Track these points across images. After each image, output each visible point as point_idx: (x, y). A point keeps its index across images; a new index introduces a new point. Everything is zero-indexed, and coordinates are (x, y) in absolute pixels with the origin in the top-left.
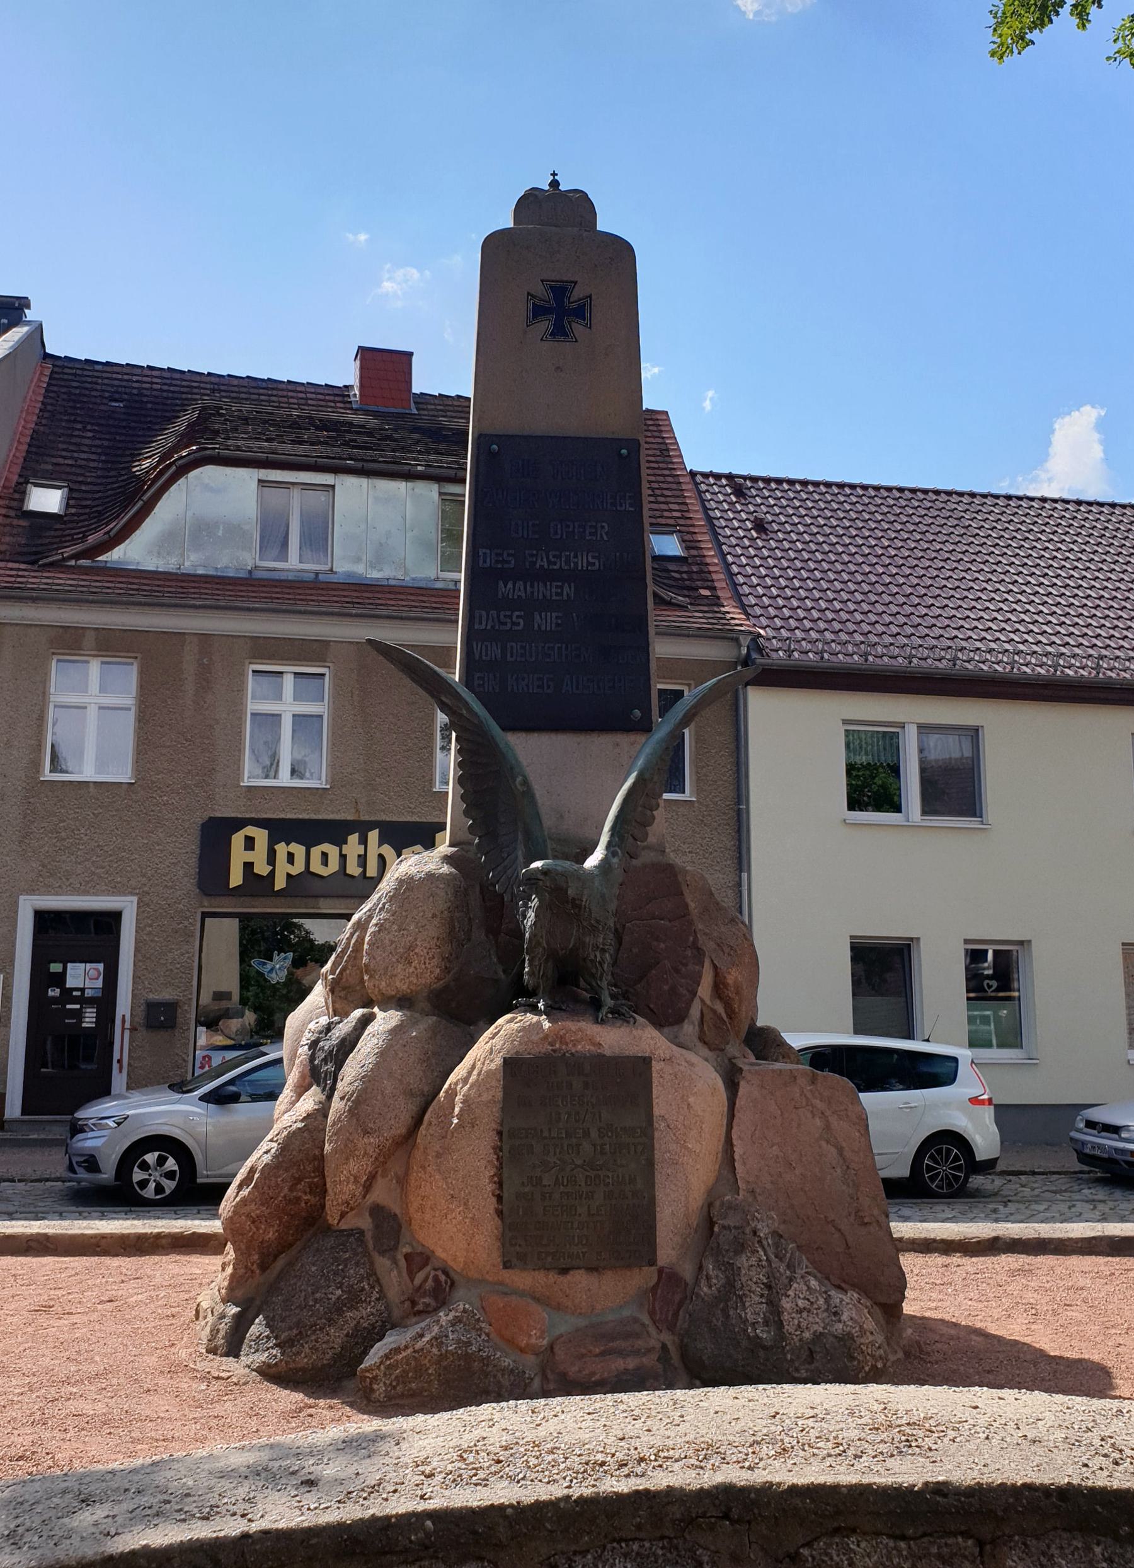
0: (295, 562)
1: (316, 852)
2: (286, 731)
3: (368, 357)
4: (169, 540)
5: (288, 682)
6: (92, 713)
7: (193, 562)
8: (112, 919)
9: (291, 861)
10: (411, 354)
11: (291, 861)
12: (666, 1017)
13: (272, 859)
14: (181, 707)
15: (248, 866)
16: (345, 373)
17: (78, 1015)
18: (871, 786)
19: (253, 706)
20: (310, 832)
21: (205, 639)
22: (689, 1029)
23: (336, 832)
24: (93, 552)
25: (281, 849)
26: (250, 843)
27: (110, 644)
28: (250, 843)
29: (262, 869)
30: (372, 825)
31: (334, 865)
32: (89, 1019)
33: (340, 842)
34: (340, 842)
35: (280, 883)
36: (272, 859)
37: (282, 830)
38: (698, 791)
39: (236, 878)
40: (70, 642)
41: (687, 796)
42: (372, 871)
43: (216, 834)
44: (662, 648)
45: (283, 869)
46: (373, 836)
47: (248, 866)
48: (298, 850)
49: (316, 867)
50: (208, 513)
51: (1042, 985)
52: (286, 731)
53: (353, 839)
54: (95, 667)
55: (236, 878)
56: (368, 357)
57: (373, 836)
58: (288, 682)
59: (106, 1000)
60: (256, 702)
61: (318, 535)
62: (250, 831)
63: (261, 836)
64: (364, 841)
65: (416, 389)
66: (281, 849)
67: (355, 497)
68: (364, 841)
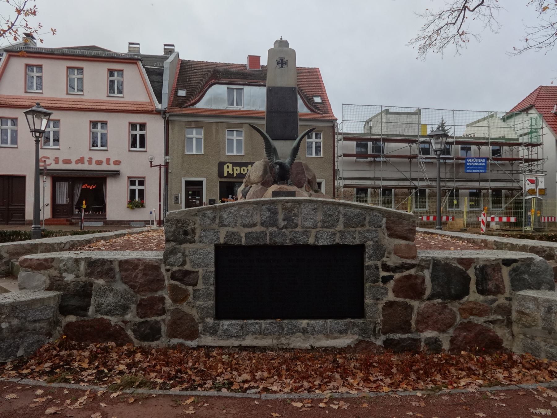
0: (235, 107)
1: (242, 169)
4: (209, 102)
5: (235, 133)
9: (237, 171)
10: (259, 57)
14: (212, 144)
15: (228, 172)
20: (241, 165)
25: (235, 168)
26: (228, 167)
28: (228, 167)
29: (231, 172)
34: (247, 167)
35: (235, 175)
37: (235, 164)
39: (226, 174)
43: (221, 165)
45: (235, 172)
47: (228, 172)
48: (238, 168)
50: (216, 96)
55: (226, 174)
58: (235, 133)
62: (228, 164)
63: (230, 165)
66: (235, 168)
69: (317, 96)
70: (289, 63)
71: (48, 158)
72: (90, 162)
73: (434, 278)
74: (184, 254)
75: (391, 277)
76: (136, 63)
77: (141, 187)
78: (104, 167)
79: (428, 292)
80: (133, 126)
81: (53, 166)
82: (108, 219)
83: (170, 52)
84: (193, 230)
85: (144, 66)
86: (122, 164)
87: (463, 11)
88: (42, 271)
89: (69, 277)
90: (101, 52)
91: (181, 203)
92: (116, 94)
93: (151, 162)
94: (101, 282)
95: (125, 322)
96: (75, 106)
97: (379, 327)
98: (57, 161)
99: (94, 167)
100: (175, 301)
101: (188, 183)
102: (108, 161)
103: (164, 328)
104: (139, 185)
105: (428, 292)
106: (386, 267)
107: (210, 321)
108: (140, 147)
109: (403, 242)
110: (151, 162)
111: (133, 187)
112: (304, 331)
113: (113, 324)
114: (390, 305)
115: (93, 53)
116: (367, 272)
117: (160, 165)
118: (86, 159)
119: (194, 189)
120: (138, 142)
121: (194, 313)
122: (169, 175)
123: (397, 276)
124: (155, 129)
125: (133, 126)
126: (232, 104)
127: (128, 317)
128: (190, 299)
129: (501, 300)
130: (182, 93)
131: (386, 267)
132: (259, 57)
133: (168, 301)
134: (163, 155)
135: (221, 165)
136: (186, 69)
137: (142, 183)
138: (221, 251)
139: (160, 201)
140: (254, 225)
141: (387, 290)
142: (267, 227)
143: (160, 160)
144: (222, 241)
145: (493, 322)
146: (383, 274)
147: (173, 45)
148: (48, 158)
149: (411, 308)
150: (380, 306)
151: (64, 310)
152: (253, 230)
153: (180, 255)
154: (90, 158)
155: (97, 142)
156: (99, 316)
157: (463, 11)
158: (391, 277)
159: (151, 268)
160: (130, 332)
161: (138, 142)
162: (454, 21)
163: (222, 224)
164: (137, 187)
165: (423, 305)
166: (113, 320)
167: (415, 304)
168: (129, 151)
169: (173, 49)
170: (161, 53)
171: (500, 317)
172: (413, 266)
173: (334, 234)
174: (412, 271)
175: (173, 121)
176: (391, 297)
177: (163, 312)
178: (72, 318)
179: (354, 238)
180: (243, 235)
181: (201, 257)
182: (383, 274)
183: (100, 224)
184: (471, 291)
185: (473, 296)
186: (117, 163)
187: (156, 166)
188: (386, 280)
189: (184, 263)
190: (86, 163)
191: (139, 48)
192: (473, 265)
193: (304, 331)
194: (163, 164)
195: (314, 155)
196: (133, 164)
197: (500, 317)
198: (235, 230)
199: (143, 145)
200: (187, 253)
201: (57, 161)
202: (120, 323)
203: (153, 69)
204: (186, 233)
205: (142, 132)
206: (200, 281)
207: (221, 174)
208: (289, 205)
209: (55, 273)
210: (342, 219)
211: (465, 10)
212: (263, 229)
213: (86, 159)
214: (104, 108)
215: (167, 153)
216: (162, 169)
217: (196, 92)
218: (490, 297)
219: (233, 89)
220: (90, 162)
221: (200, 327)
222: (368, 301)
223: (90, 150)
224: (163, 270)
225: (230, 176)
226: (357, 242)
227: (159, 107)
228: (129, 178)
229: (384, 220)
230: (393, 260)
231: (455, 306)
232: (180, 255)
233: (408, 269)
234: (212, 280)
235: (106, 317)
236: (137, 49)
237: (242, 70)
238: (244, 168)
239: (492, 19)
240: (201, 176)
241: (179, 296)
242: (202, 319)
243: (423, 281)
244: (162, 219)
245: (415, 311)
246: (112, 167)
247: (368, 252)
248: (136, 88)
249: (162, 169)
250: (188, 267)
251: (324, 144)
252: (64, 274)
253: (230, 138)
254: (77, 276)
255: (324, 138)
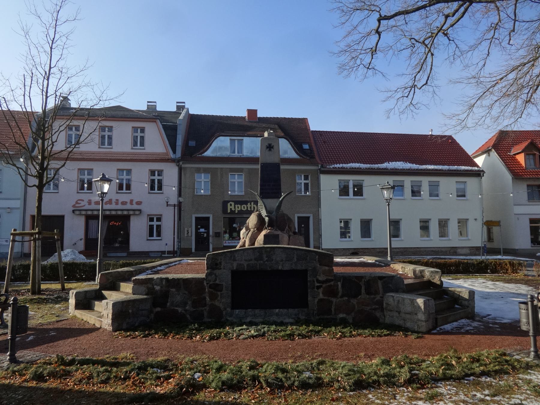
0: (236, 154)
1: (242, 206)
2: (236, 185)
3: (249, 111)
4: (215, 150)
5: (236, 176)
6: (203, 182)
7: (218, 154)
8: (208, 218)
9: (238, 208)
10: (257, 110)
11: (238, 208)
12: (282, 230)
13: (235, 208)
14: (218, 184)
15: (231, 209)
16: (245, 114)
17: (203, 235)
18: (344, 191)
19: (230, 180)
20: (241, 203)
21: (222, 169)
22: (285, 232)
23: (246, 203)
24: (201, 154)
25: (236, 206)
26: (231, 205)
27: (206, 171)
28: (231, 205)
29: (233, 209)
30: (252, 201)
31: (246, 208)
32: (205, 235)
33: (247, 204)
34: (247, 204)
35: (236, 212)
36: (235, 208)
37: (236, 203)
38: (312, 192)
39: (229, 211)
40: (198, 170)
41: (211, 216)
42: (252, 209)
43: (225, 204)
44: (30, 312)
45: (237, 209)
46: (252, 203)
47: (231, 209)
48: (239, 206)
49: (243, 209)
50: (221, 145)
51: (374, 228)
52: (236, 185)
53: (249, 204)
54: (203, 175)
55: (229, 211)
56: (249, 111)
57: (252, 203)
58: (236, 176)
59: (208, 233)
60: (231, 180)
61: (240, 149)
62: (231, 203)
63: (233, 204)
64: (251, 204)
65: (258, 116)
66: (236, 206)
67: (247, 141)
68: (251, 204)
69: (305, 143)
70: (275, 147)
71: (83, 200)
72: (117, 203)
73: (343, 286)
74: (215, 275)
75: (321, 286)
76: (155, 122)
77: (159, 223)
78: (128, 206)
79: (340, 294)
80: (153, 173)
81: (87, 207)
82: (131, 250)
83: (183, 107)
84: (220, 263)
85: (161, 122)
86: (143, 204)
87: (413, 89)
88: (144, 285)
89: (157, 288)
90: (126, 113)
91: (191, 236)
92: (139, 147)
93: (167, 202)
94: (174, 290)
95: (186, 311)
96: (106, 157)
97: (315, 312)
98: (90, 202)
99: (120, 207)
100: (211, 299)
101: (197, 219)
102: (131, 201)
103: (206, 314)
104: (157, 221)
105: (340, 294)
106: (318, 281)
107: (229, 310)
108: (158, 190)
109: (327, 268)
110: (167, 202)
111: (152, 223)
112: (277, 315)
113: (180, 311)
114: (321, 300)
115: (120, 113)
116: (309, 284)
117: (175, 205)
118: (114, 201)
119: (202, 222)
120: (156, 185)
121: (221, 306)
122: (182, 212)
123: (324, 285)
124: (170, 174)
125: (153, 173)
126: (234, 152)
127: (187, 308)
128: (219, 298)
129: (378, 297)
130: (192, 143)
131: (318, 281)
132: (257, 110)
133: (208, 299)
134: (177, 196)
135: (225, 204)
136: (195, 121)
137: (159, 220)
138: (235, 274)
139: (174, 235)
140: (251, 260)
141: (319, 293)
142: (257, 261)
143: (174, 200)
144: (235, 269)
145: (375, 309)
146: (317, 284)
147: (184, 103)
148: (83, 200)
149: (332, 302)
150: (316, 301)
151: (154, 305)
152: (251, 262)
153: (213, 276)
154: (117, 200)
155: (124, 186)
156: (173, 308)
157: (413, 89)
158: (321, 286)
159: (199, 281)
160: (188, 316)
161: (156, 185)
162: (406, 95)
163: (235, 260)
164: (155, 223)
165: (338, 301)
166: (180, 310)
167: (334, 300)
168: (149, 193)
169: (184, 106)
170: (174, 109)
171: (377, 307)
172: (332, 280)
173: (292, 264)
174: (332, 283)
175: (185, 168)
176: (321, 296)
177: (205, 305)
178: (158, 309)
179: (300, 267)
180: (246, 265)
181: (225, 276)
182: (317, 284)
183: (125, 254)
184: (362, 293)
185: (364, 296)
186: (139, 203)
187: (171, 205)
188: (318, 287)
189: (216, 280)
190: (114, 204)
191: (156, 106)
192: (363, 280)
193: (277, 315)
194: (176, 204)
195: (303, 194)
196: (153, 204)
197: (377, 307)
198: (242, 263)
199: (160, 188)
200: (217, 274)
201: (90, 202)
202: (183, 311)
203: (167, 123)
204: (217, 264)
205: (160, 178)
206: (224, 289)
207: (225, 210)
208: (268, 250)
209: (150, 286)
210: (295, 257)
211: (415, 87)
212: (256, 262)
213: (114, 201)
214: (129, 158)
215: (180, 195)
216: (176, 208)
217: (206, 143)
218: (372, 296)
219: (235, 140)
220: (117, 203)
221: (224, 313)
222: (310, 298)
223: (117, 193)
224: (205, 284)
225: (232, 212)
226: (304, 268)
227: (172, 155)
228: (148, 215)
229: (317, 257)
230: (321, 278)
231: (354, 301)
232: (213, 276)
233: (330, 282)
234: (230, 288)
235: (176, 308)
236: (154, 107)
237: (241, 123)
238: (244, 205)
239: (435, 95)
240: (208, 213)
241: (213, 297)
242: (225, 309)
243: (338, 288)
244: (176, 249)
245: (334, 303)
246: (135, 207)
247: (309, 273)
248: (155, 141)
249: (176, 208)
250: (217, 282)
251: (312, 184)
252: (155, 286)
253: (233, 180)
254: (161, 287)
255: (311, 180)
